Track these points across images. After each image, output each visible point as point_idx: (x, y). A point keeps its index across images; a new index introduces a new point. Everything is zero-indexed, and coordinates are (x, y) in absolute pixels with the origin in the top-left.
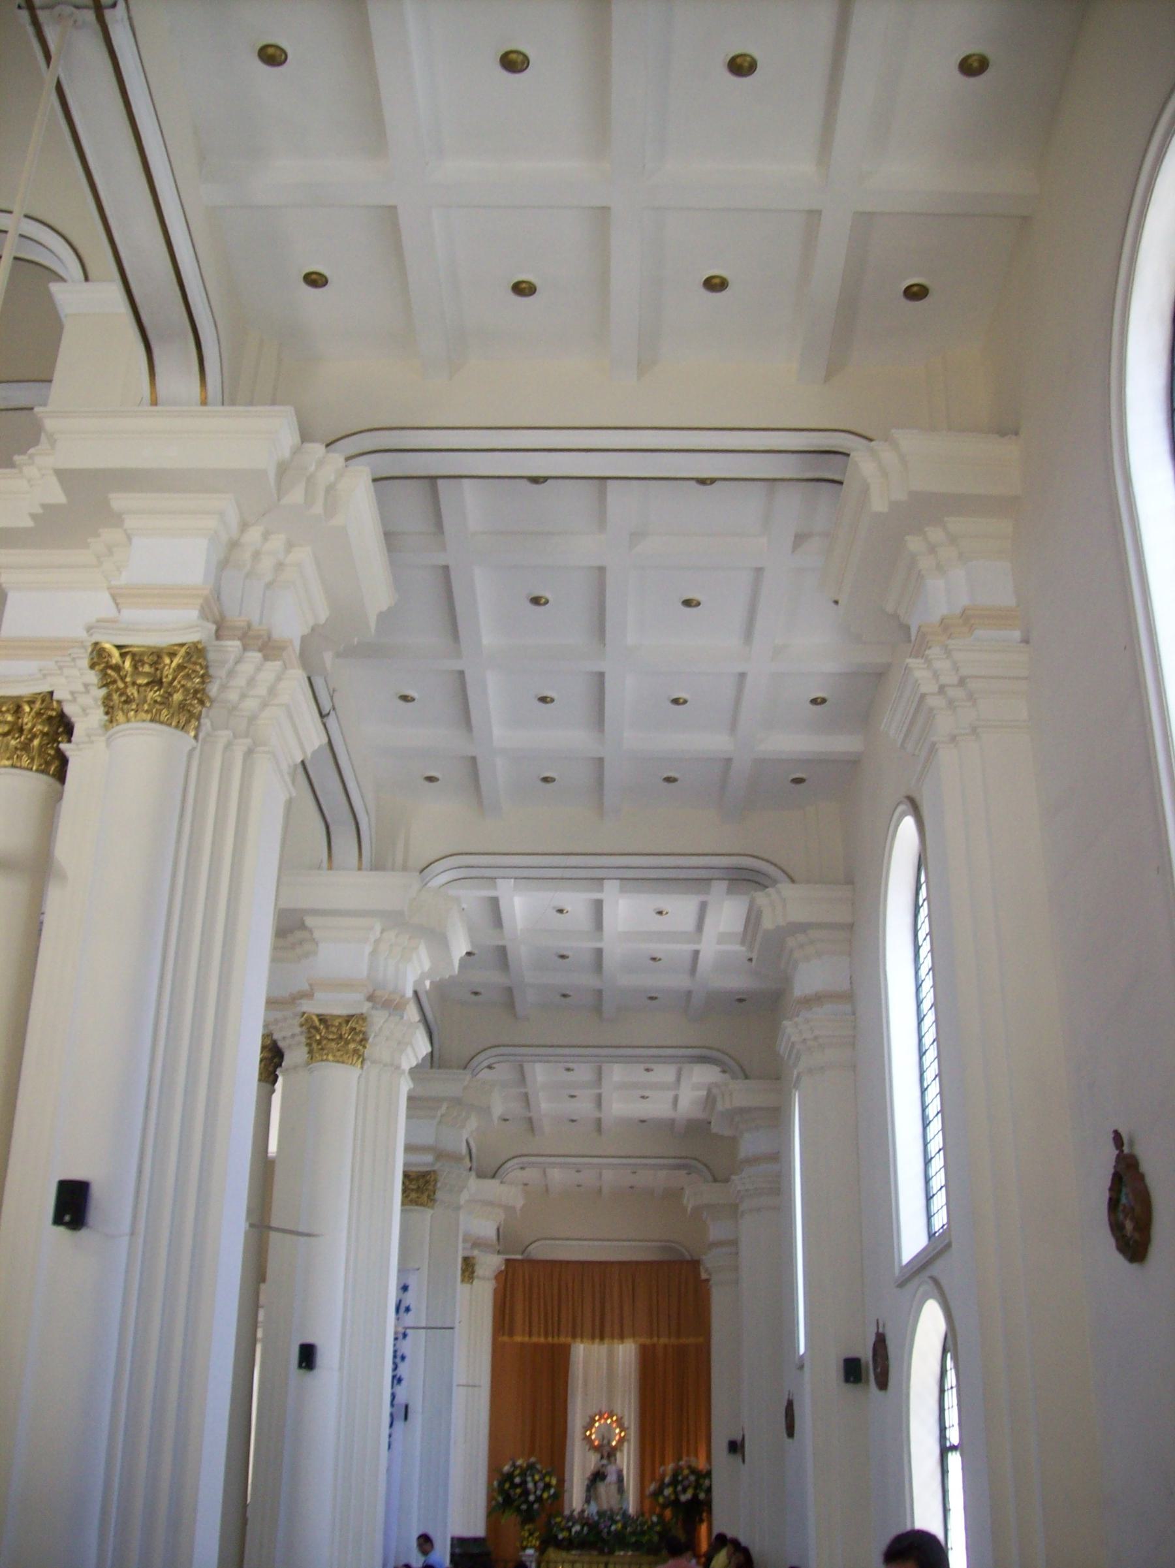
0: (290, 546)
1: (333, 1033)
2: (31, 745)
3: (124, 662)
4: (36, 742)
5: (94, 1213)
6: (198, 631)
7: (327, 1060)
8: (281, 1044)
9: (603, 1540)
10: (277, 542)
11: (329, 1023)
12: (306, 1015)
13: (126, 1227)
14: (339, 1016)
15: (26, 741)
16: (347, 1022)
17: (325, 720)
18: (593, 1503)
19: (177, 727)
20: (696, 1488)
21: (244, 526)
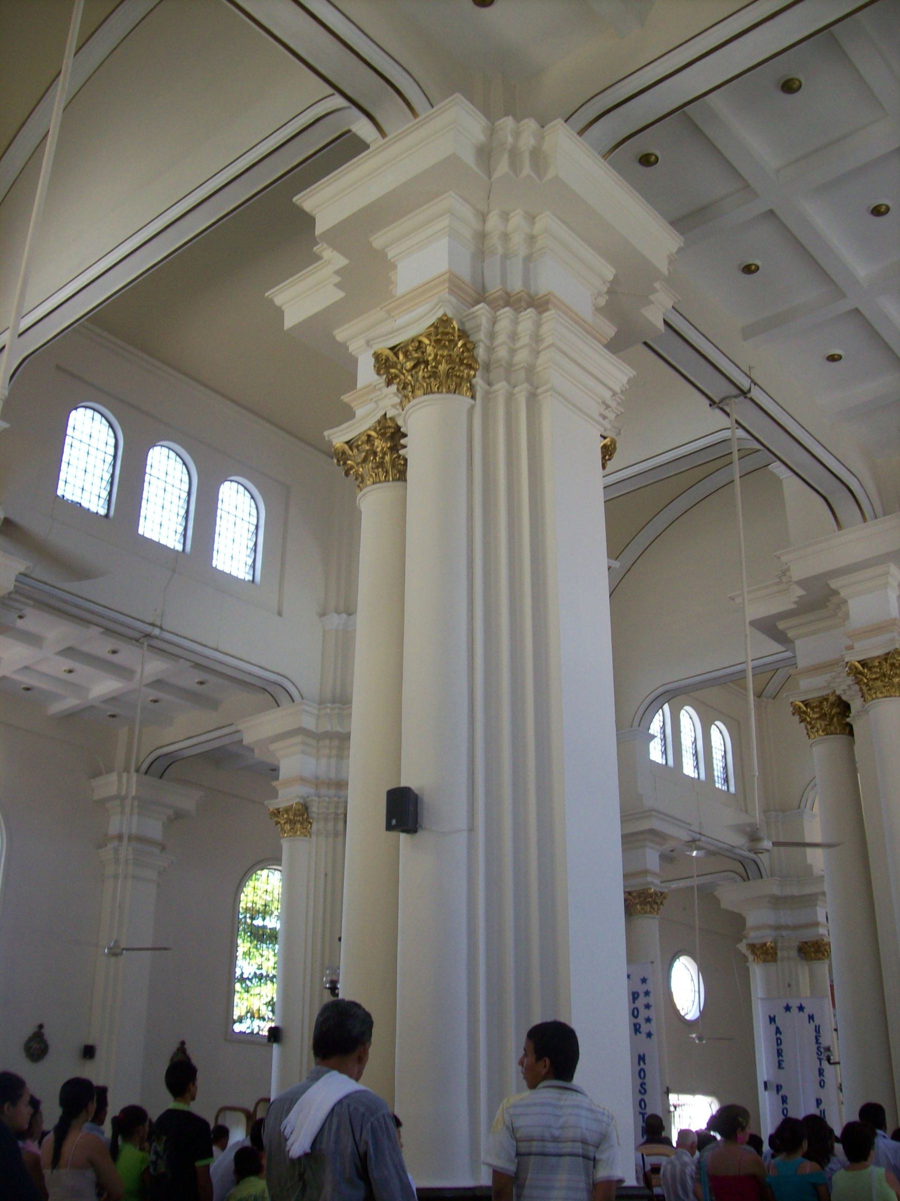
0: (531, 219)
1: (876, 672)
2: (385, 461)
3: (398, 358)
4: (387, 458)
5: (426, 817)
6: (441, 307)
7: (877, 698)
8: (844, 698)
10: (517, 219)
11: (870, 665)
12: (849, 665)
13: (462, 822)
14: (878, 657)
15: (381, 460)
16: (886, 660)
17: (749, 395)
19: (448, 391)
21: (483, 217)
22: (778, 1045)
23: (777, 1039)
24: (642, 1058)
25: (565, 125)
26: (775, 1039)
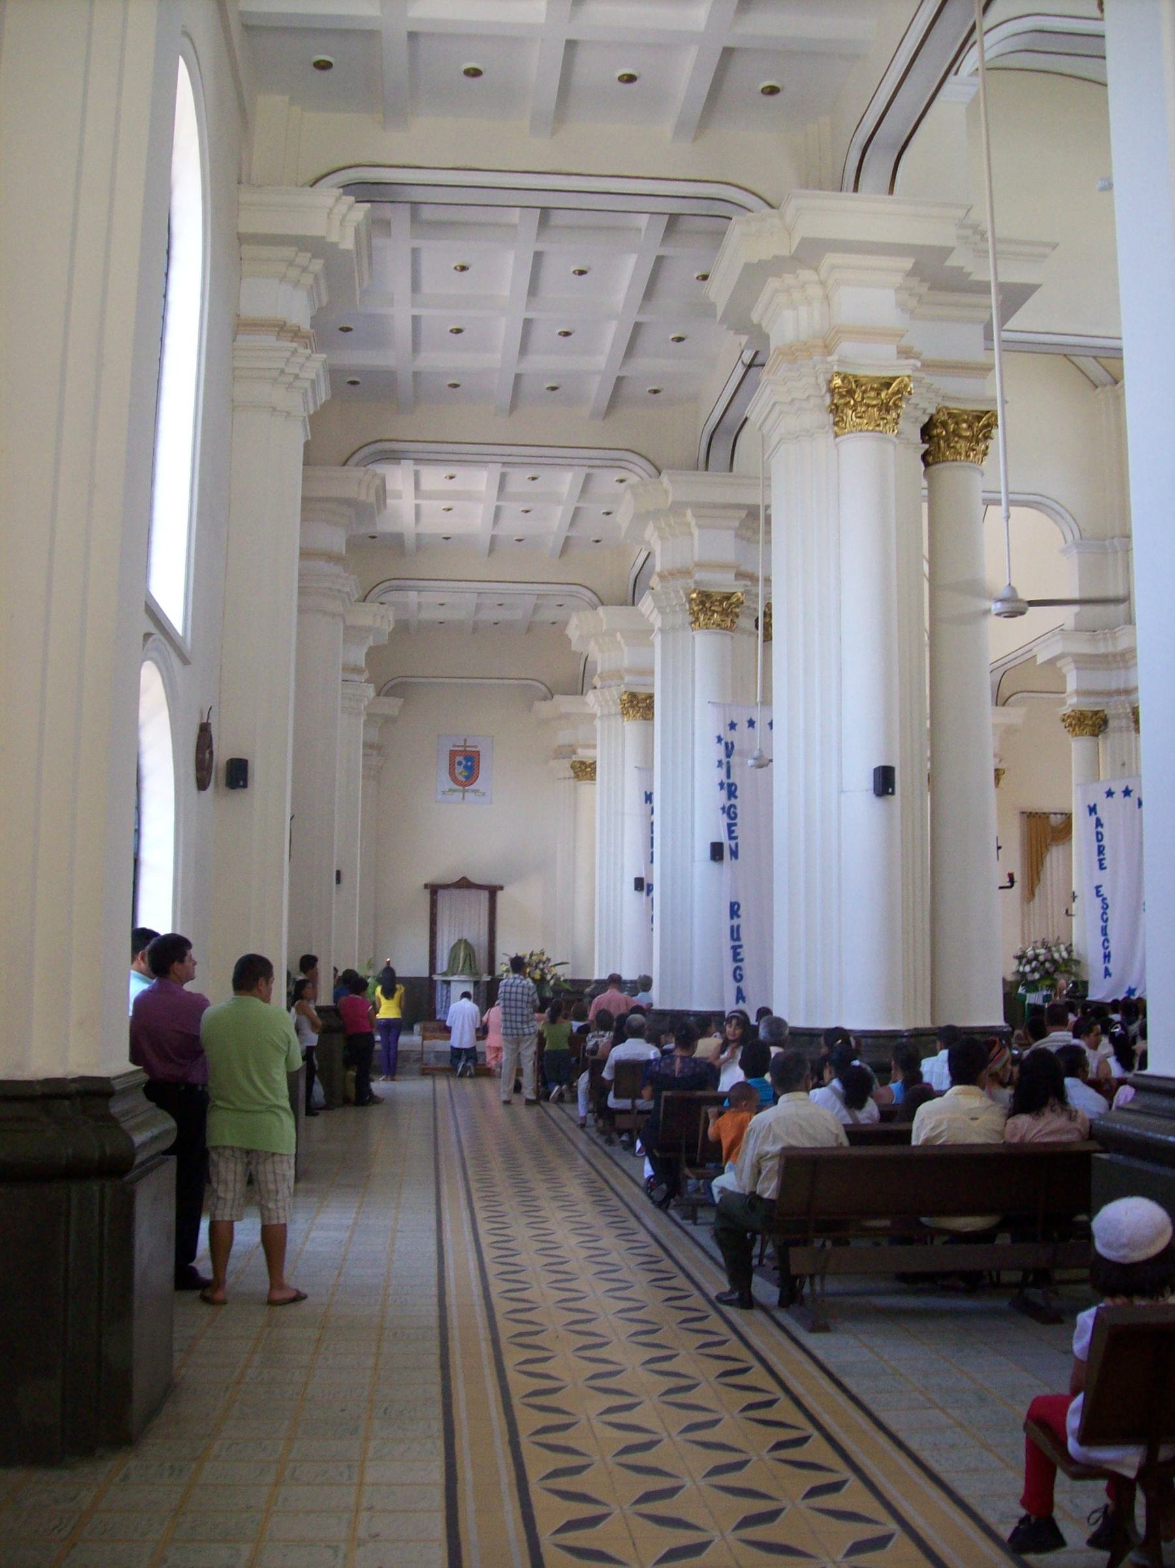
22: (1099, 841)
23: (1098, 833)
24: (734, 909)
25: (842, 194)
26: (1095, 834)
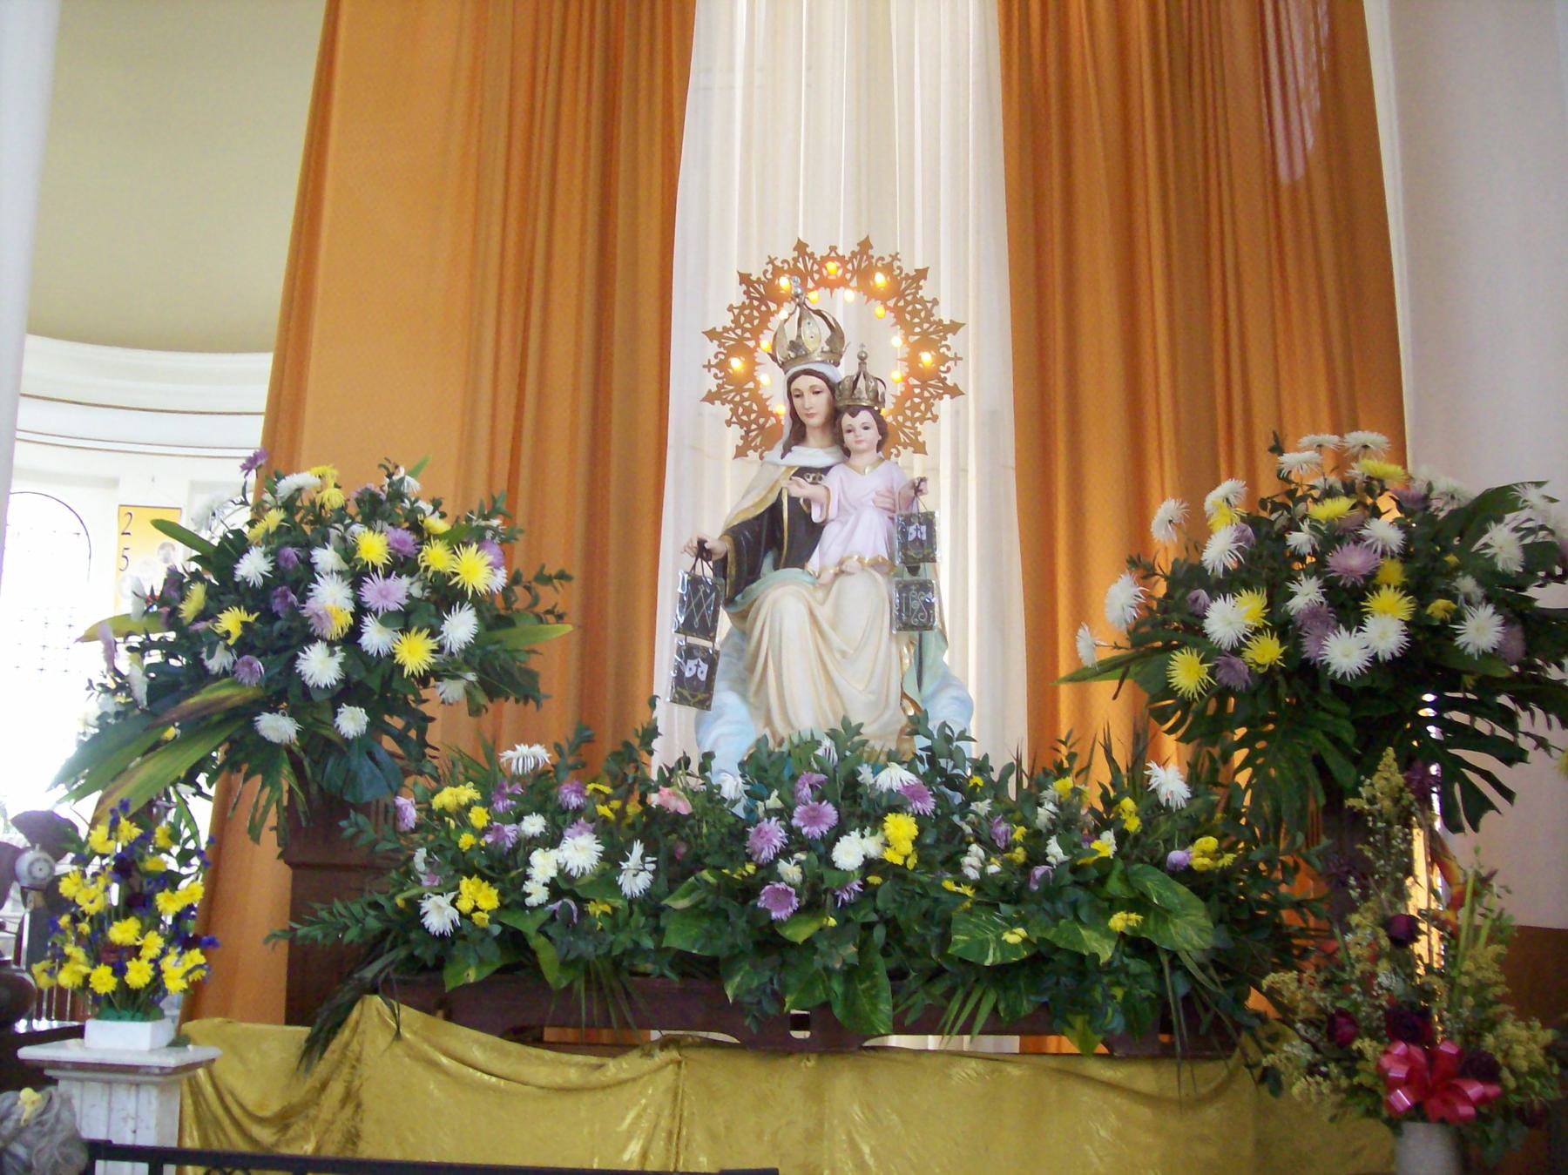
9: (769, 941)
18: (725, 696)
20: (1420, 587)
